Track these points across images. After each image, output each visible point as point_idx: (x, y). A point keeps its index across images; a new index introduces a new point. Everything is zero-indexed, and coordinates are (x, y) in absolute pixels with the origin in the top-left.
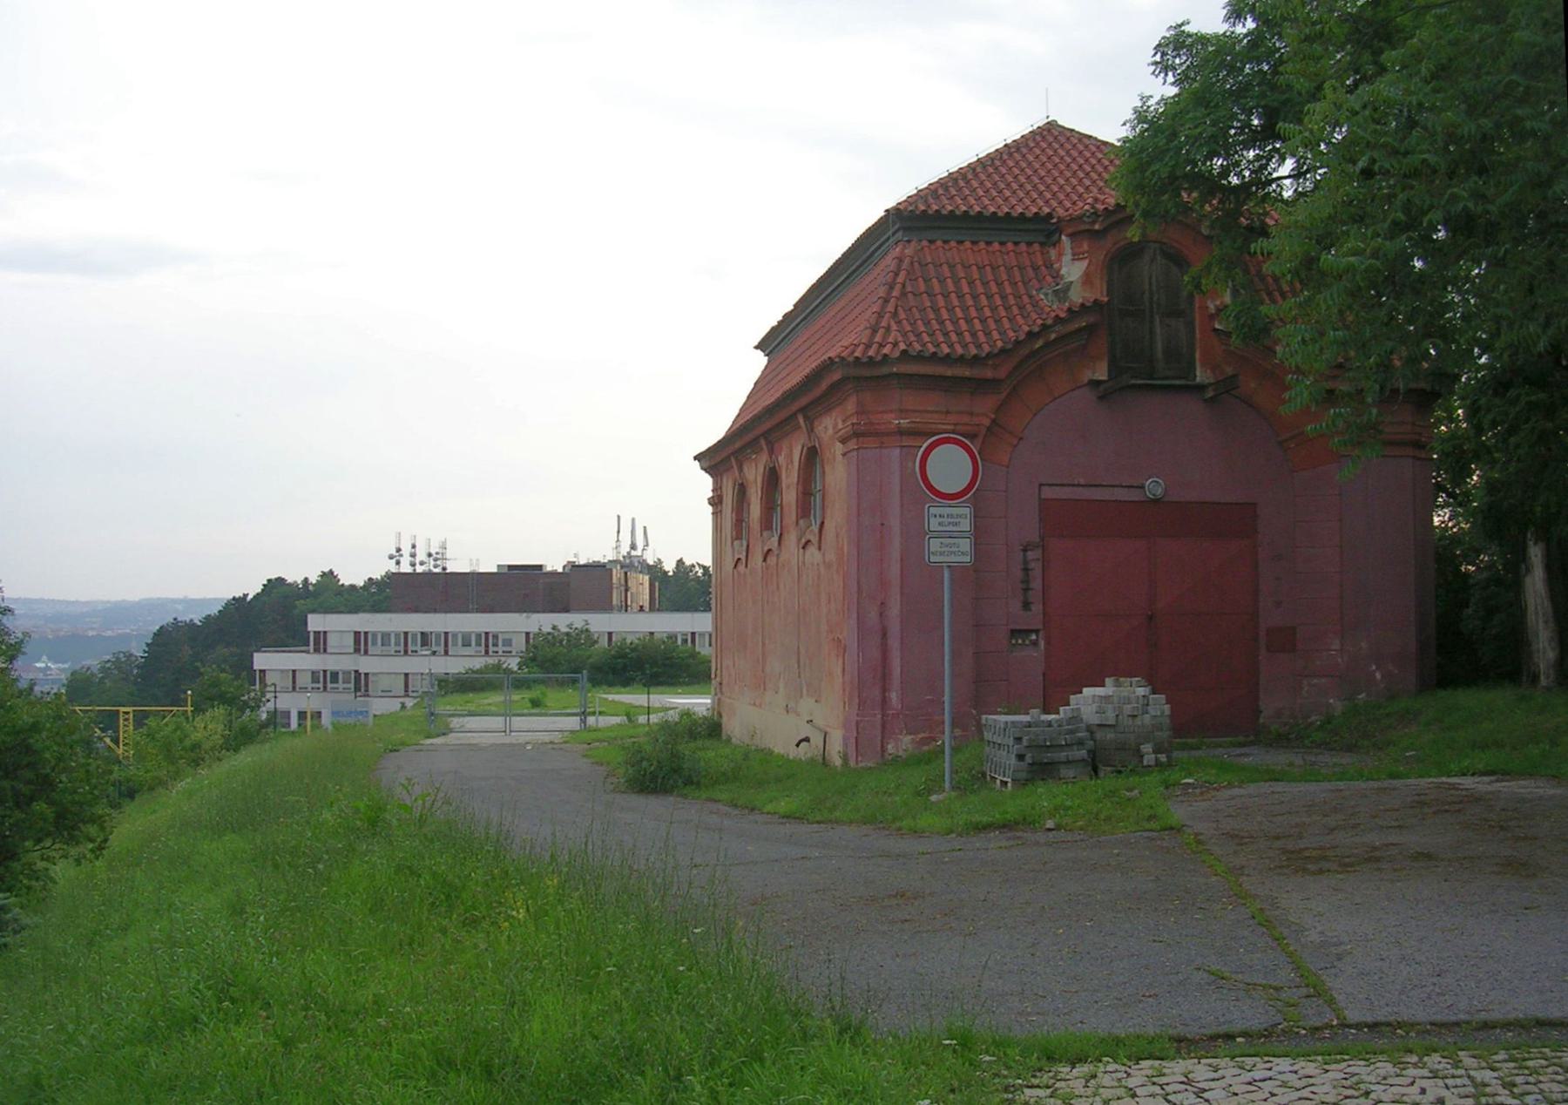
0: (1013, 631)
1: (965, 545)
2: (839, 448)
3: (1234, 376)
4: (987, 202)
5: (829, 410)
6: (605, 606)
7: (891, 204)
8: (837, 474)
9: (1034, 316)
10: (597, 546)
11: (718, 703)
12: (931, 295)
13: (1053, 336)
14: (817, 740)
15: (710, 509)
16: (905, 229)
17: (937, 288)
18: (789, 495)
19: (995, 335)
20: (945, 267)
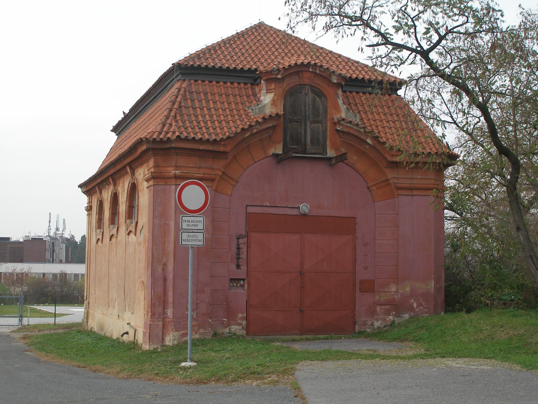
0: (231, 279)
1: (200, 236)
2: (146, 184)
3: (346, 153)
4: (224, 62)
5: (141, 165)
6: (42, 260)
7: (175, 61)
8: (144, 198)
9: (246, 120)
10: (40, 230)
11: (87, 314)
12: (194, 109)
13: (255, 131)
14: (131, 333)
15: (86, 213)
16: (182, 74)
17: (197, 105)
18: (123, 208)
19: (226, 129)
20: (202, 94)
